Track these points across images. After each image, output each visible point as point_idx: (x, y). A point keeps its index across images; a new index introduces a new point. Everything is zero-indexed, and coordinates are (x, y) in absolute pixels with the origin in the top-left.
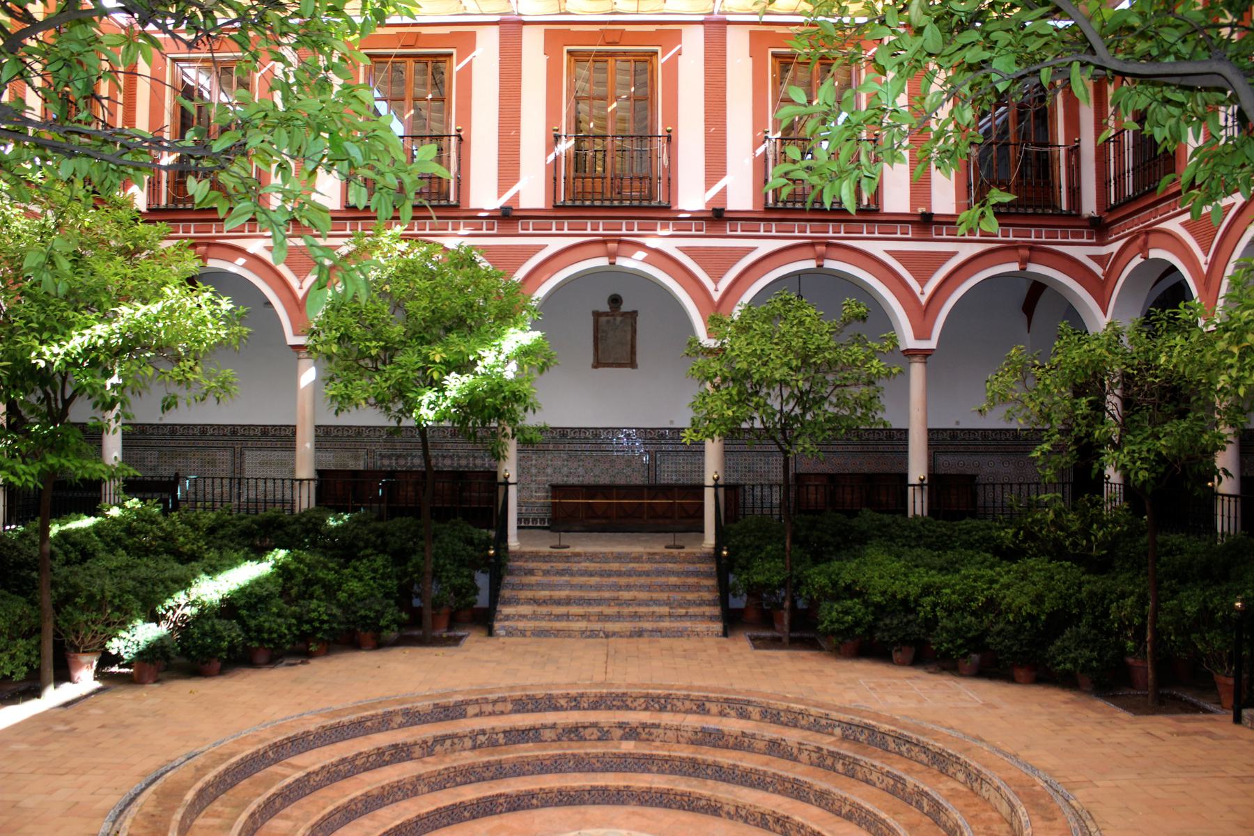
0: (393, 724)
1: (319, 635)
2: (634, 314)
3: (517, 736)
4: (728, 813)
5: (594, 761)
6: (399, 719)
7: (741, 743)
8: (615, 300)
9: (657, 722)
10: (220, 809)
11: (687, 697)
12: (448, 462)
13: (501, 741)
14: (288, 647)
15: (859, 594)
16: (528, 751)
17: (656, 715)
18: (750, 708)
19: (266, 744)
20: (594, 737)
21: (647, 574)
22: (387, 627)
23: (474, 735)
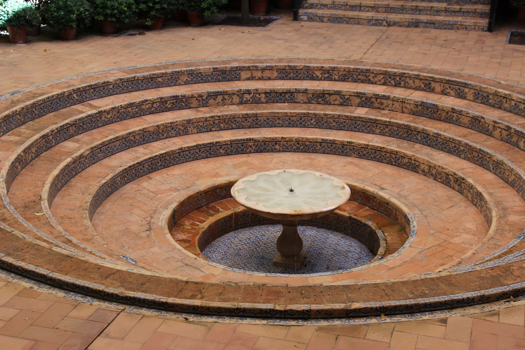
0: (179, 81)
1: (153, 13)
3: (274, 97)
4: (423, 171)
5: (331, 120)
6: (185, 78)
7: (451, 117)
9: (387, 94)
10: (23, 131)
11: (417, 77)
13: (263, 100)
14: (127, 21)
16: (282, 108)
17: (391, 89)
18: (466, 90)
19: (71, 88)
20: (337, 102)
22: (208, 9)
23: (241, 94)
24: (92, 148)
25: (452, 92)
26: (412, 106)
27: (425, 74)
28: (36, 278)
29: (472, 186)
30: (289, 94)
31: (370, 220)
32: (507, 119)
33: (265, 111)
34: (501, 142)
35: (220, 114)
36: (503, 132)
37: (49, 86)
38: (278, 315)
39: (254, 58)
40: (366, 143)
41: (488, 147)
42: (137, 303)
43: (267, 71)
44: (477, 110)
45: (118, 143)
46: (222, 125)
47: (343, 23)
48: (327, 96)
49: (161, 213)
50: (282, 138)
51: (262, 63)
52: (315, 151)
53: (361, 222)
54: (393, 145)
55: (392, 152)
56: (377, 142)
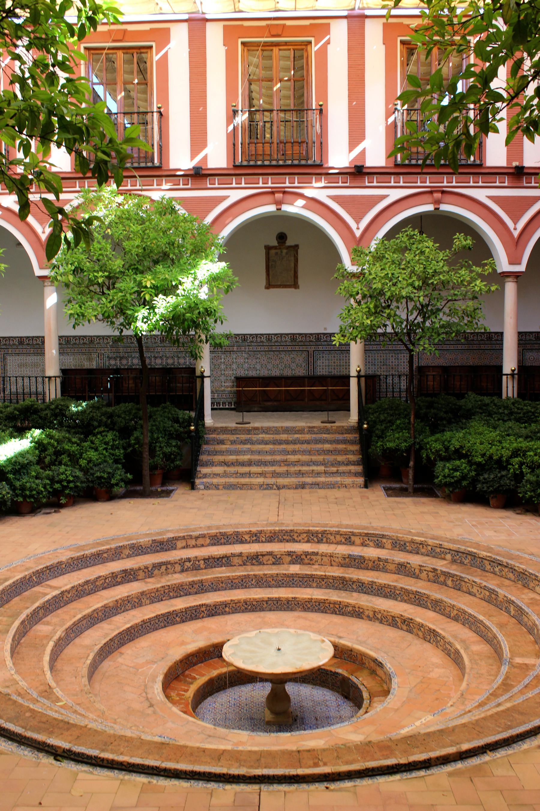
0: (123, 555)
1: (67, 492)
2: (296, 247)
3: (212, 562)
4: (368, 616)
5: (270, 579)
6: (127, 552)
7: (377, 565)
8: (282, 237)
11: (338, 533)
12: (159, 361)
14: (44, 500)
15: (465, 456)
17: (315, 545)
18: (384, 540)
20: (270, 562)
21: (308, 442)
22: (117, 485)
23: (182, 562)
24: (66, 630)
25: (371, 544)
26: (340, 560)
27: (344, 530)
28: (146, 771)
29: (423, 625)
30: (226, 559)
31: (338, 667)
32: (429, 562)
33: (209, 577)
34: (429, 583)
35: (169, 584)
36: (430, 573)
37: (8, 570)
38: (403, 769)
39: (182, 528)
40: (310, 597)
41: (421, 588)
42: (266, 780)
43: (200, 539)
44: (400, 557)
45: (85, 621)
46: (171, 594)
47: (237, 489)
48: (260, 557)
49: (152, 687)
50: (231, 600)
51: (194, 531)
52: (262, 610)
53: (331, 671)
54: (334, 596)
55: (335, 603)
56: (318, 595)
